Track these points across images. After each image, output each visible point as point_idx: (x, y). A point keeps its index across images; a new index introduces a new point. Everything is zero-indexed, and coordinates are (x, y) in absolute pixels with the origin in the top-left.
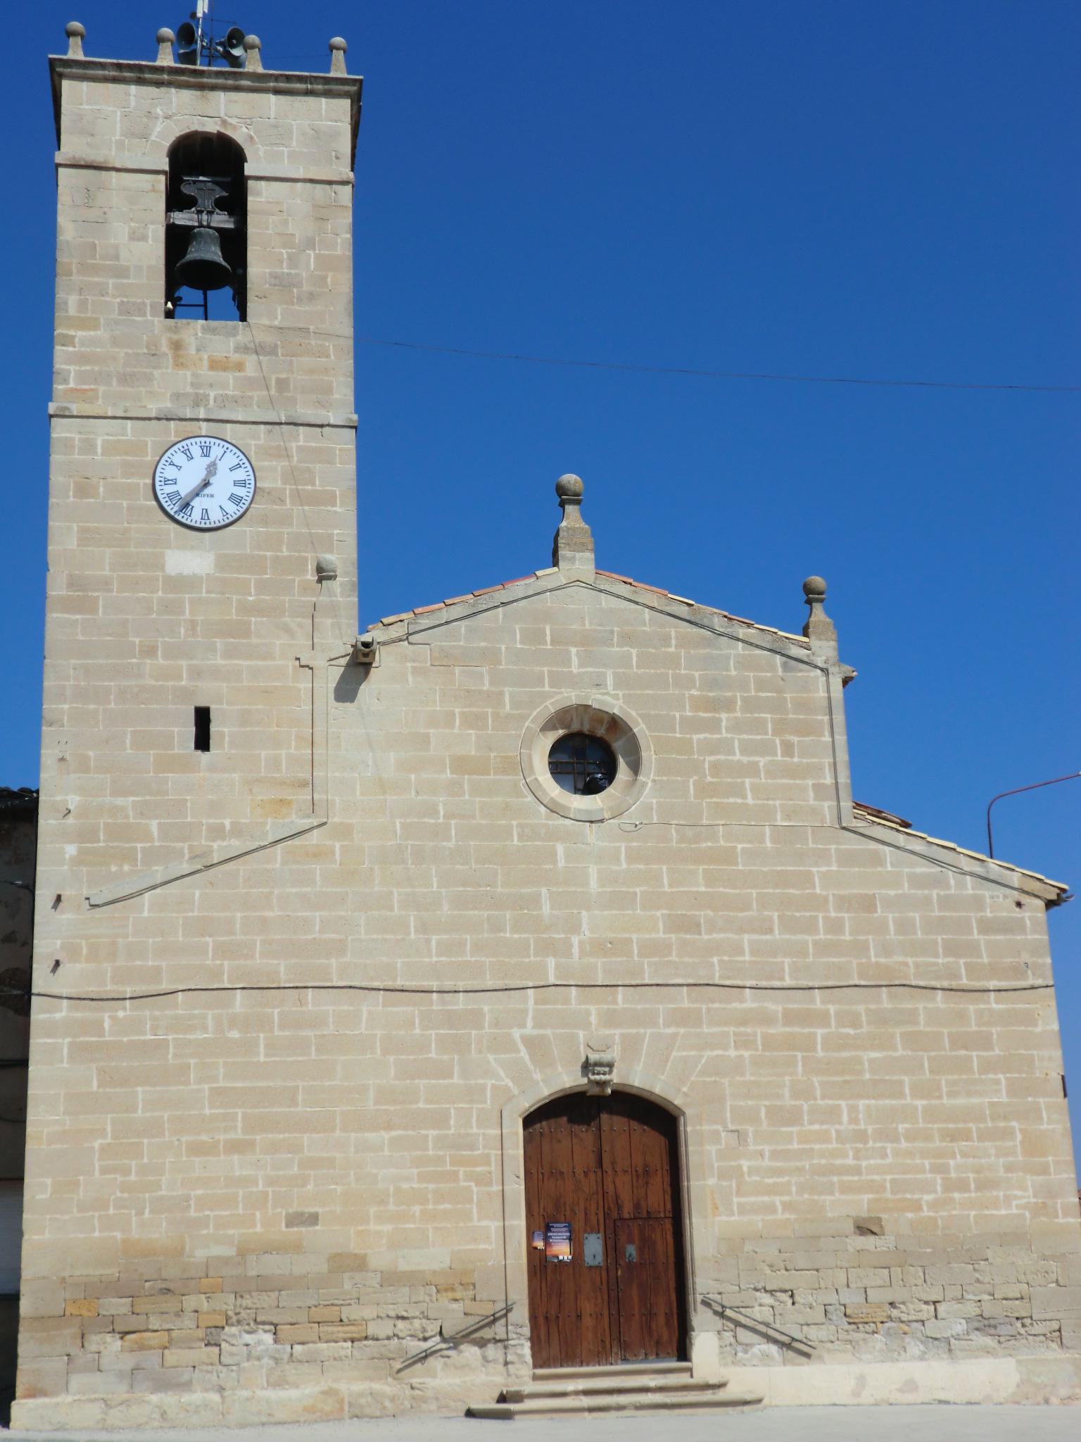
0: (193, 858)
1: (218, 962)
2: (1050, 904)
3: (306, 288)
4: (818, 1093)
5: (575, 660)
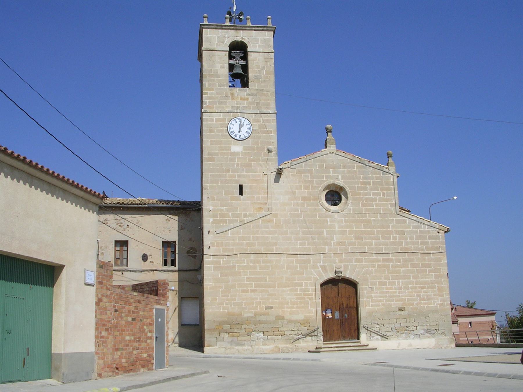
0: (240, 222)
2: (445, 232)
5: (331, 172)
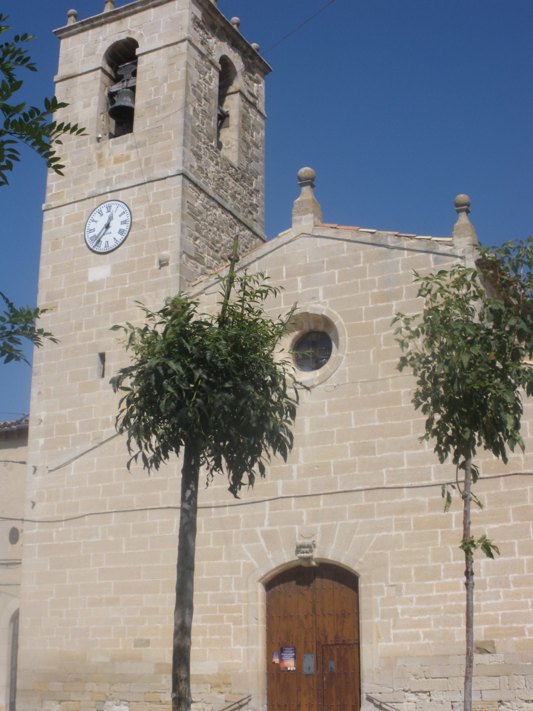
1: (104, 498)
3: (162, 104)
4: (452, 557)
5: (300, 285)
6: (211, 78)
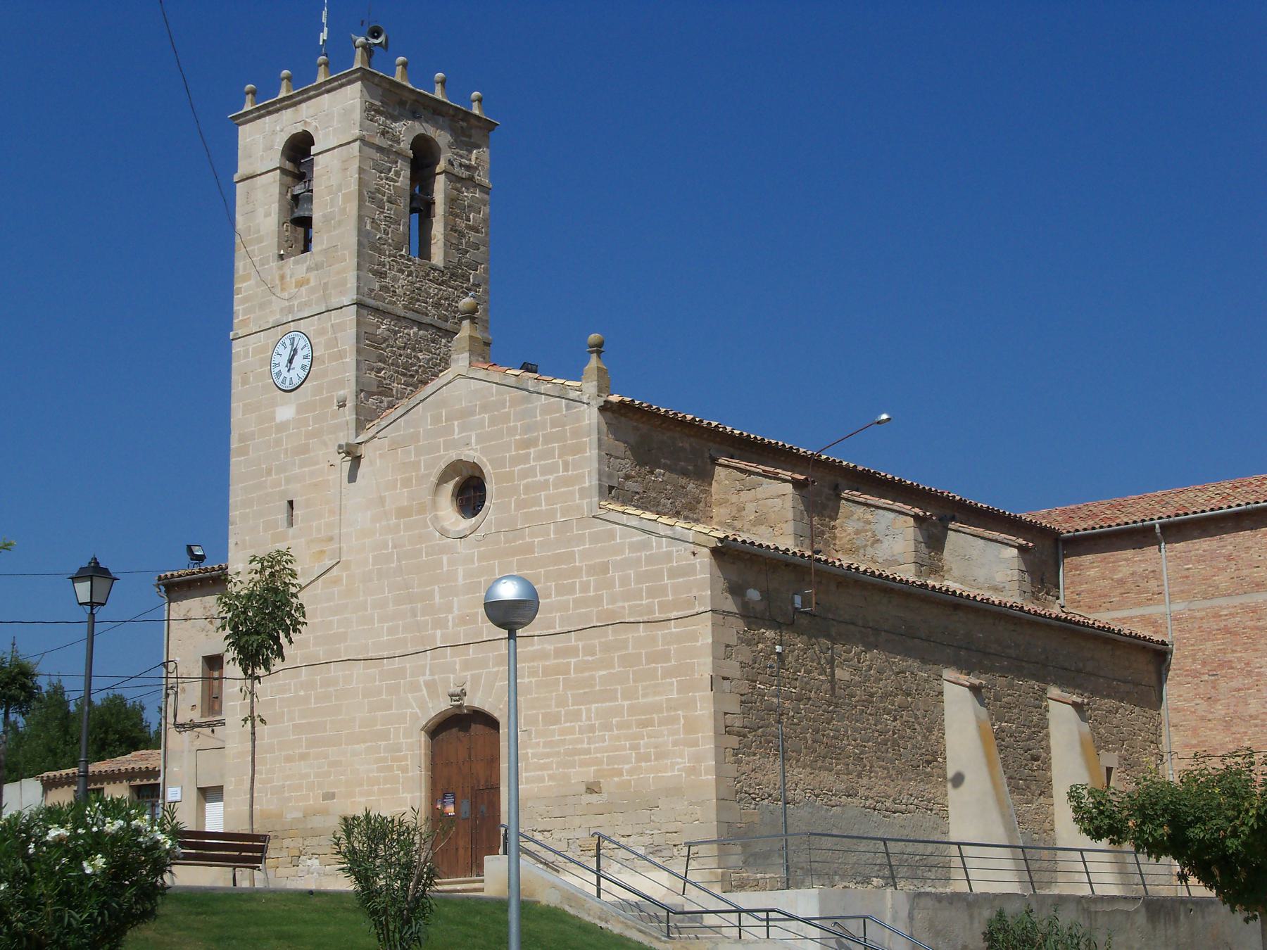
6: (398, 174)
